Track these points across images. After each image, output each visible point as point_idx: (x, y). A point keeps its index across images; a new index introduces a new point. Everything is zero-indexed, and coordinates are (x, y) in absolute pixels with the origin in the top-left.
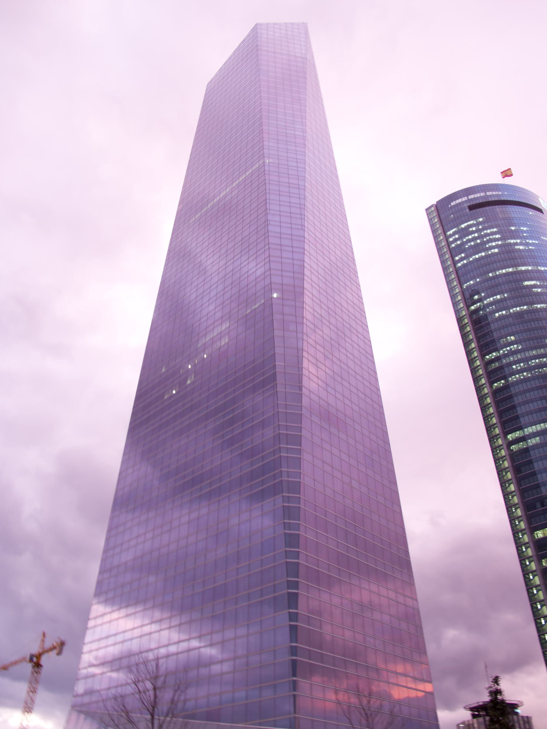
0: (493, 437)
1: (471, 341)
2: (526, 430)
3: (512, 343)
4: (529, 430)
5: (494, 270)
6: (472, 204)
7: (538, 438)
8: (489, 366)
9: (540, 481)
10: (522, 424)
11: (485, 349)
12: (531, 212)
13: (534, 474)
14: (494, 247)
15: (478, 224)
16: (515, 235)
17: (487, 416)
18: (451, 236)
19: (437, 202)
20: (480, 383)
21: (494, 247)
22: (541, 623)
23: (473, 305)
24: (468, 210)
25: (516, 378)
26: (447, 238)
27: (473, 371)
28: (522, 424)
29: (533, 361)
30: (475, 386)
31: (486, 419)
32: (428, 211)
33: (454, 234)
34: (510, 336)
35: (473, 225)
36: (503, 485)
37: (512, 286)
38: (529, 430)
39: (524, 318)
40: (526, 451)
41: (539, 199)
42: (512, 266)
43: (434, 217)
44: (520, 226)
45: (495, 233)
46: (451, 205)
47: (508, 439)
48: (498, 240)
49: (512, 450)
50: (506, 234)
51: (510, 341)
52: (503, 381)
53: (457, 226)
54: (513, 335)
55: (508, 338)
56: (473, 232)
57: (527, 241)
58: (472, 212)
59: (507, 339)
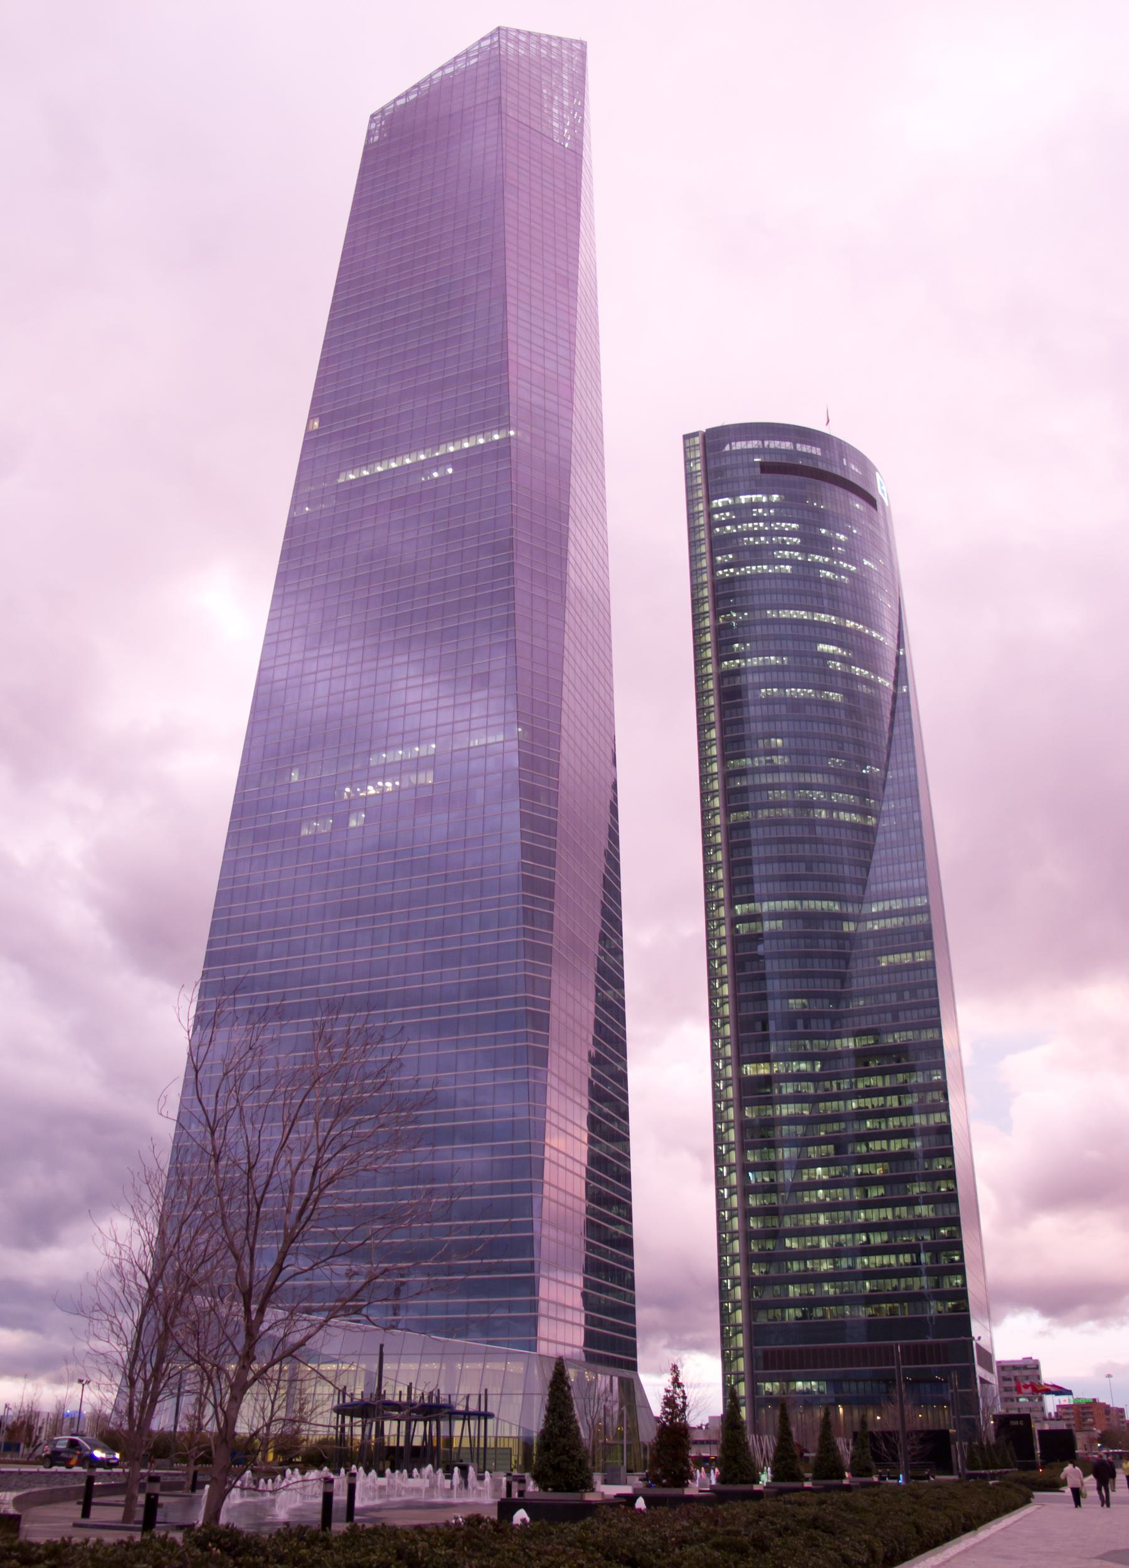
0: (703, 709)
1: (710, 726)
2: (749, 660)
3: (775, 752)
4: (767, 907)
5: (777, 607)
6: (768, 459)
7: (780, 922)
8: (731, 780)
9: (769, 989)
10: (769, 1011)
11: (723, 649)
12: (858, 505)
13: (762, 977)
14: (785, 561)
15: (769, 505)
16: (825, 545)
17: (699, 614)
18: (718, 510)
19: (707, 430)
20: (696, 509)
21: (785, 561)
22: (723, 1195)
23: (757, 1060)
24: (758, 470)
25: (751, 569)
26: (710, 512)
27: (697, 632)
28: (769, 1011)
29: (778, 524)
30: (694, 626)
31: (699, 679)
32: (687, 441)
33: (726, 508)
34: (776, 738)
35: (758, 504)
36: (699, 663)
37: (817, 852)
38: (767, 907)
39: (815, 834)
40: (757, 938)
41: (877, 474)
42: (807, 609)
43: (695, 459)
44: (835, 531)
45: (792, 533)
46: (731, 447)
47: (735, 911)
48: (793, 548)
49: (737, 931)
50: (811, 542)
51: (773, 746)
52: (731, 556)
53: (734, 496)
54: (782, 738)
55: (773, 740)
56: (758, 519)
57: (841, 563)
58: (764, 476)
59: (770, 742)
